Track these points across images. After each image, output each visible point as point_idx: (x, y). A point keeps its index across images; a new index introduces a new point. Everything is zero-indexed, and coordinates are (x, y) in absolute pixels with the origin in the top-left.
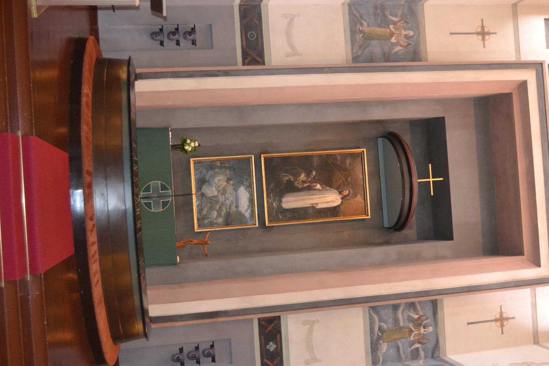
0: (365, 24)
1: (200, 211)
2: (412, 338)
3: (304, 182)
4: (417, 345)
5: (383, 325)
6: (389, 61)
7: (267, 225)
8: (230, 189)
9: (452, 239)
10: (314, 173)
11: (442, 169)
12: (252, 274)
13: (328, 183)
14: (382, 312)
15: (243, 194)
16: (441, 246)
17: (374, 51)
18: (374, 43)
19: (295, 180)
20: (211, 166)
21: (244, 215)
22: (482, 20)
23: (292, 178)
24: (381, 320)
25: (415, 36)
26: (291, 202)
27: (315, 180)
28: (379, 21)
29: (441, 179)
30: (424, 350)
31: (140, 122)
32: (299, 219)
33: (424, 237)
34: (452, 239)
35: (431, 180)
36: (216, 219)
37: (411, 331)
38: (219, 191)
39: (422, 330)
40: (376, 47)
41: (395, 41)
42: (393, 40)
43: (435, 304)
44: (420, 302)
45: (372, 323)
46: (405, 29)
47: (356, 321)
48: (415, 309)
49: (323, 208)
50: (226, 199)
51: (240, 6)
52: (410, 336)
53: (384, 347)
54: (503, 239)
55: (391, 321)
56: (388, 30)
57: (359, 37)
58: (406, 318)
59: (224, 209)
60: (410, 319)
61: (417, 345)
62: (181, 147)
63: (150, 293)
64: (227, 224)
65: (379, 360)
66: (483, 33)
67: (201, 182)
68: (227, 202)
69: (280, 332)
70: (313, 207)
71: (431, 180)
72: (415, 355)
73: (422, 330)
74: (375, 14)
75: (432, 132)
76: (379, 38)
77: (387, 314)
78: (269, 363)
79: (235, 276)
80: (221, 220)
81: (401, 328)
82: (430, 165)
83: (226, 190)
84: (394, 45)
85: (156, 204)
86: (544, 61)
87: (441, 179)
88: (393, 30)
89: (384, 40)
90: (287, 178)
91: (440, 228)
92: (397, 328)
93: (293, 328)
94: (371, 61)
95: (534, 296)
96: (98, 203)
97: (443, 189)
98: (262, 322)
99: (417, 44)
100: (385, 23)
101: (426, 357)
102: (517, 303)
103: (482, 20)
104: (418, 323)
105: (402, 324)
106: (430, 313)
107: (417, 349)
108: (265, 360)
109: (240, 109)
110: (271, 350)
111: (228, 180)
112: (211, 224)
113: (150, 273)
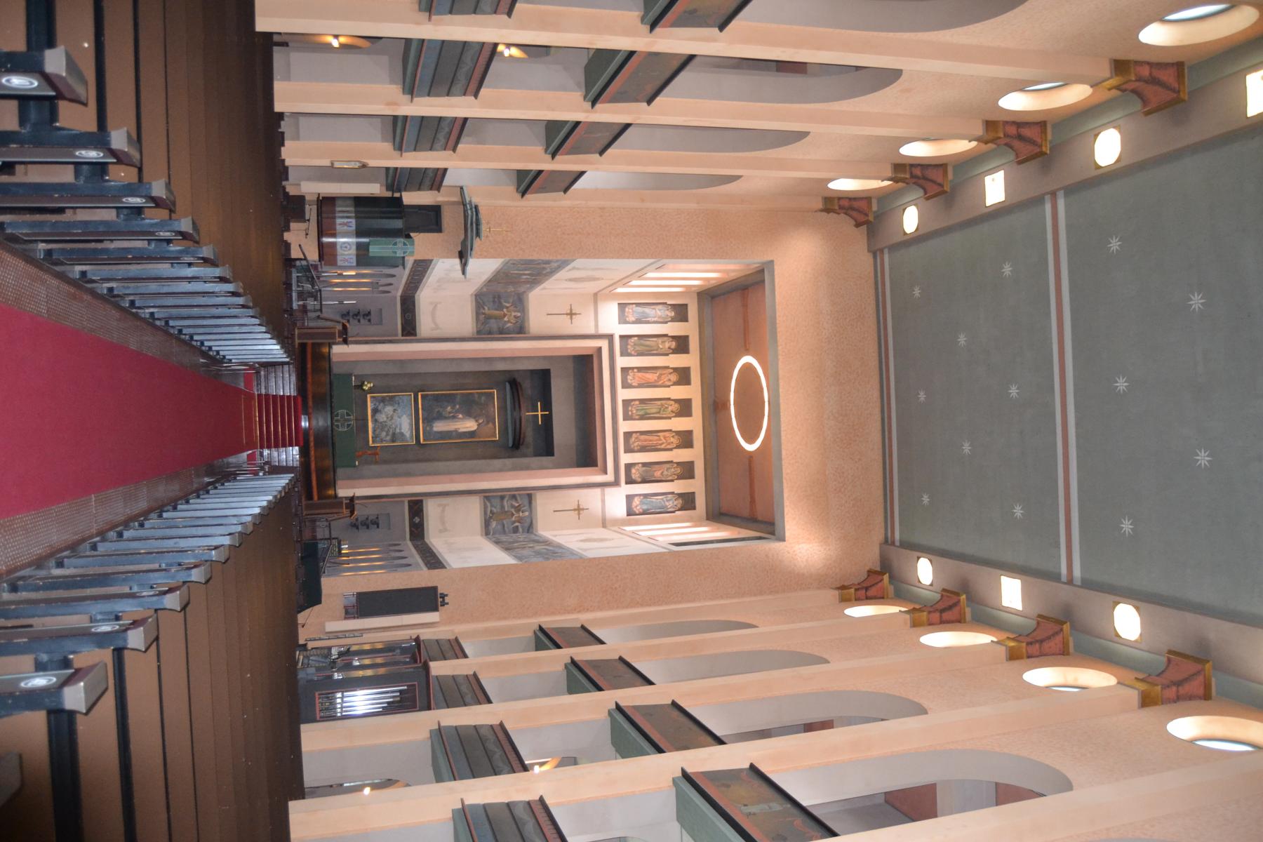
1: (374, 431)
6: (502, 334)
11: (547, 405)
12: (408, 474)
13: (469, 414)
20: (383, 400)
26: (439, 426)
27: (458, 411)
31: (336, 370)
33: (538, 454)
40: (493, 324)
43: (530, 497)
47: (474, 507)
53: (494, 524)
54: (587, 456)
57: (482, 317)
60: (513, 506)
62: (360, 387)
64: (393, 441)
66: (571, 314)
67: (375, 411)
70: (456, 431)
72: (516, 530)
75: (543, 377)
76: (496, 318)
77: (496, 502)
79: (396, 475)
85: (343, 425)
91: (546, 448)
92: (503, 512)
93: (432, 509)
94: (490, 333)
95: (603, 495)
97: (548, 420)
99: (523, 322)
100: (500, 307)
102: (591, 499)
104: (518, 509)
106: (526, 502)
109: (402, 362)
112: (382, 441)
113: (340, 471)
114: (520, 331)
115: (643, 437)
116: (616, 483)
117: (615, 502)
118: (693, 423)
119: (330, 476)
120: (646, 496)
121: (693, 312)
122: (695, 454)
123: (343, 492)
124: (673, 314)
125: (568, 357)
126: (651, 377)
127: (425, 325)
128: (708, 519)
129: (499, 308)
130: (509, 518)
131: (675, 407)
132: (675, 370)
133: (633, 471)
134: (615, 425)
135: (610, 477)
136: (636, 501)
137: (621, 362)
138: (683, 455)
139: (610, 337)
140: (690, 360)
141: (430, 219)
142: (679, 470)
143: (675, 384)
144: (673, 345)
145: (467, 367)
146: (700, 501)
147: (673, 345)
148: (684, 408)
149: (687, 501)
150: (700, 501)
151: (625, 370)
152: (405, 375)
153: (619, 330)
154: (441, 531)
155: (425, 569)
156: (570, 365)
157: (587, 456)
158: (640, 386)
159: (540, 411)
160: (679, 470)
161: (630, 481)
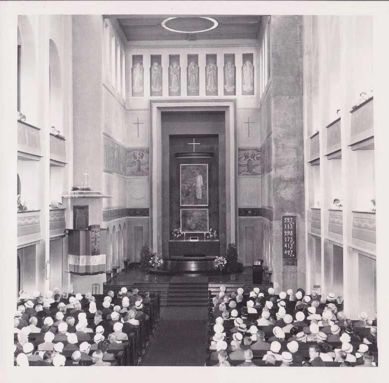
2: (252, 159)
4: (255, 158)
11: (190, 137)
14: (241, 171)
16: (221, 139)
24: (244, 171)
26: (199, 196)
43: (239, 150)
44: (239, 156)
45: (244, 175)
54: (217, 115)
60: (245, 160)
67: (190, 229)
77: (242, 169)
92: (247, 165)
93: (244, 205)
94: (148, 169)
96: (193, 270)
106: (243, 152)
107: (257, 158)
116: (234, 102)
125: (162, 124)
126: (174, 79)
127: (142, 204)
132: (170, 63)
133: (228, 90)
134: (203, 98)
139: (151, 102)
141: (81, 211)
142: (156, 64)
146: (248, 51)
147: (156, 64)
149: (248, 57)
151: (170, 94)
157: (217, 115)
161: (234, 93)
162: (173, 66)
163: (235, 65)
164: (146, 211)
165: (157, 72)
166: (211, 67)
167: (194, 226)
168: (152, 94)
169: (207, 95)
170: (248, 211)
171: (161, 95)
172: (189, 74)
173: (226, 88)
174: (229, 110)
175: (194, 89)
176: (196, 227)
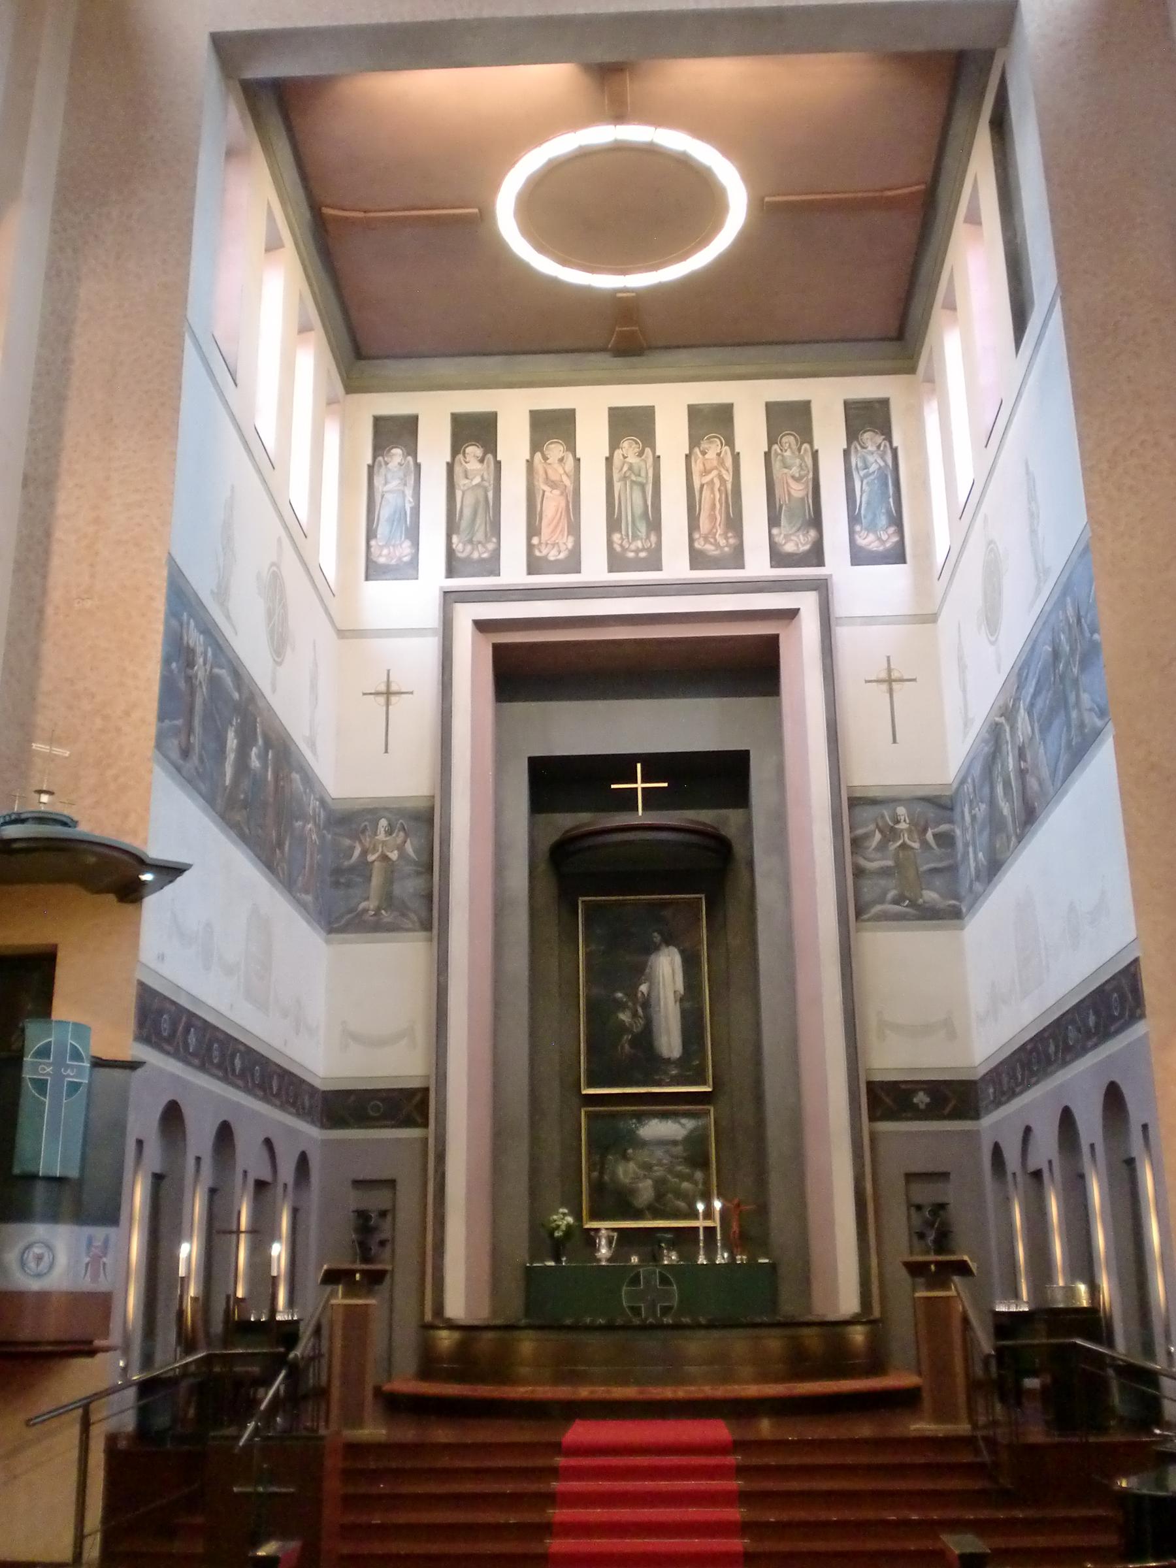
0: (363, 905)
2: (916, 845)
3: (635, 1015)
4: (929, 836)
5: (892, 894)
6: (431, 864)
7: (710, 1090)
8: (644, 1155)
9: (747, 752)
10: (620, 995)
11: (622, 766)
15: (656, 1129)
17: (411, 890)
18: (397, 890)
19: (631, 1032)
21: (692, 1132)
22: (364, 694)
23: (627, 1037)
25: (389, 815)
26: (670, 1041)
27: (632, 992)
28: (359, 880)
29: (639, 765)
30: (938, 824)
32: (702, 1028)
34: (747, 752)
35: (640, 785)
36: (696, 1183)
37: (904, 846)
38: (645, 1177)
39: (903, 826)
40: (408, 887)
41: (396, 852)
42: (394, 855)
43: (855, 802)
45: (885, 917)
46: (376, 834)
48: (868, 836)
49: (684, 982)
50: (660, 1164)
51: (323, 1126)
52: (912, 848)
53: (930, 896)
54: (747, 666)
55: (883, 882)
56: (376, 863)
57: (387, 916)
58: (879, 855)
59: (679, 1168)
60: (882, 847)
61: (929, 836)
63: (1078, 1305)
64: (704, 1164)
65: (954, 906)
68: (665, 1161)
69: (895, 1084)
71: (640, 785)
72: (946, 840)
73: (903, 826)
74: (348, 885)
75: (556, 782)
78: (951, 1105)
80: (699, 1175)
81: (898, 864)
82: (613, 786)
83: (645, 1162)
84: (403, 854)
86: (441, 588)
87: (639, 765)
88: (376, 855)
89: (392, 872)
90: (627, 1046)
91: (722, 777)
93: (892, 1059)
94: (429, 897)
95: (851, 620)
97: (656, 765)
98: (878, 1114)
99: (401, 813)
100: (363, 869)
101: (951, 821)
103: (364, 694)
104: (890, 833)
105: (890, 863)
106: (867, 813)
107: (935, 836)
108: (946, 1111)
110: (927, 1100)
111: (625, 1158)
114: (425, 821)
115: (704, 524)
116: (822, 587)
117: (868, 592)
118: (670, 402)
119: (812, 1339)
120: (853, 519)
121: (394, 404)
122: (749, 400)
123: (848, 1303)
124: (397, 451)
125: (499, 719)
126: (552, 504)
127: (401, 1066)
128: (912, 370)
129: (361, 873)
130: (921, 859)
131: (629, 448)
132: (536, 446)
133: (789, 548)
134: (674, 588)
135: (806, 603)
136: (868, 541)
137: (513, 572)
138: (750, 430)
139: (450, 598)
140: (513, 409)
142: (789, 440)
143: (571, 447)
144: (474, 451)
145: (519, 961)
146: (867, 388)
148: (632, 425)
150: (867, 388)
152: (534, 1125)
153: (433, 573)
154: (952, 1035)
155: (1139, 1029)
156: (519, 709)
157: (747, 666)
158: (575, 529)
159: (638, 814)
160: (789, 440)
161: (816, 556)
162: (545, 458)
163: (816, 447)
164: (418, 1098)
165: (477, 480)
166: (711, 454)
167: (646, 1192)
168: (453, 567)
169: (693, 567)
170: (914, 1092)
171: (496, 572)
172: (617, 486)
173: (780, 539)
174: (799, 628)
175: (639, 544)
176: (660, 1196)
